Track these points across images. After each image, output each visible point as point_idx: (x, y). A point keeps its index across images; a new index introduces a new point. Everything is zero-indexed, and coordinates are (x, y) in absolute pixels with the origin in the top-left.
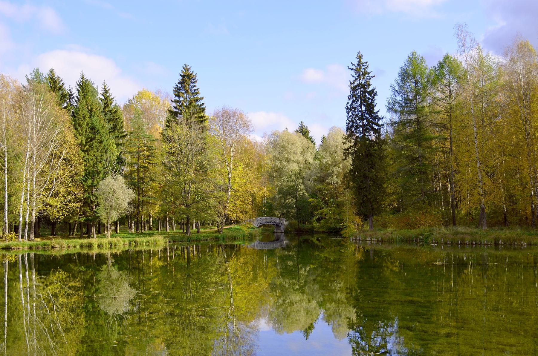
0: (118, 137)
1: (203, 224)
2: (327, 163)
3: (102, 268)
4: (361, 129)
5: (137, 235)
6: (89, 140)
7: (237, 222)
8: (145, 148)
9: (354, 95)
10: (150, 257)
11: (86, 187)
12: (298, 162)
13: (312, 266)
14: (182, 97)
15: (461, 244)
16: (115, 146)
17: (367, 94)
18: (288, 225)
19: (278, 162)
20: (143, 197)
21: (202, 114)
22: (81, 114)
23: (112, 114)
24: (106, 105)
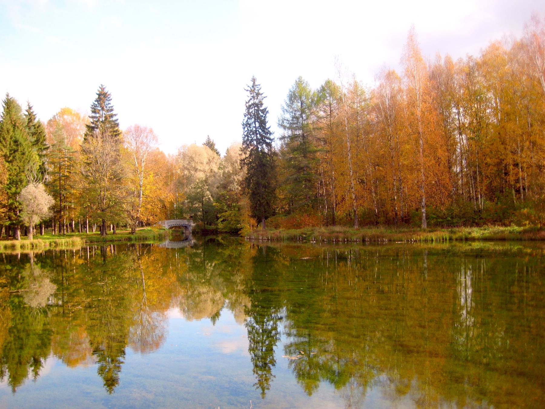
0: (41, 149)
1: (118, 226)
2: (229, 172)
3: (26, 266)
4: (255, 143)
5: (59, 236)
6: (13, 152)
7: (148, 224)
8: (66, 159)
9: (249, 113)
10: (73, 256)
11: (10, 194)
12: (204, 171)
13: (216, 262)
14: (98, 113)
15: (335, 241)
16: (38, 157)
17: (260, 112)
18: (195, 226)
19: (187, 171)
20: (65, 202)
21: (117, 128)
22: (5, 128)
23: (35, 128)
24: (30, 120)
